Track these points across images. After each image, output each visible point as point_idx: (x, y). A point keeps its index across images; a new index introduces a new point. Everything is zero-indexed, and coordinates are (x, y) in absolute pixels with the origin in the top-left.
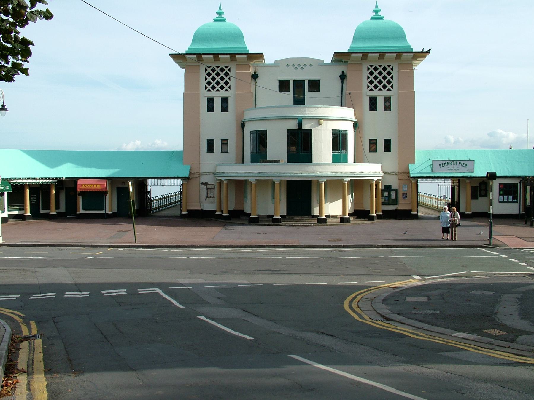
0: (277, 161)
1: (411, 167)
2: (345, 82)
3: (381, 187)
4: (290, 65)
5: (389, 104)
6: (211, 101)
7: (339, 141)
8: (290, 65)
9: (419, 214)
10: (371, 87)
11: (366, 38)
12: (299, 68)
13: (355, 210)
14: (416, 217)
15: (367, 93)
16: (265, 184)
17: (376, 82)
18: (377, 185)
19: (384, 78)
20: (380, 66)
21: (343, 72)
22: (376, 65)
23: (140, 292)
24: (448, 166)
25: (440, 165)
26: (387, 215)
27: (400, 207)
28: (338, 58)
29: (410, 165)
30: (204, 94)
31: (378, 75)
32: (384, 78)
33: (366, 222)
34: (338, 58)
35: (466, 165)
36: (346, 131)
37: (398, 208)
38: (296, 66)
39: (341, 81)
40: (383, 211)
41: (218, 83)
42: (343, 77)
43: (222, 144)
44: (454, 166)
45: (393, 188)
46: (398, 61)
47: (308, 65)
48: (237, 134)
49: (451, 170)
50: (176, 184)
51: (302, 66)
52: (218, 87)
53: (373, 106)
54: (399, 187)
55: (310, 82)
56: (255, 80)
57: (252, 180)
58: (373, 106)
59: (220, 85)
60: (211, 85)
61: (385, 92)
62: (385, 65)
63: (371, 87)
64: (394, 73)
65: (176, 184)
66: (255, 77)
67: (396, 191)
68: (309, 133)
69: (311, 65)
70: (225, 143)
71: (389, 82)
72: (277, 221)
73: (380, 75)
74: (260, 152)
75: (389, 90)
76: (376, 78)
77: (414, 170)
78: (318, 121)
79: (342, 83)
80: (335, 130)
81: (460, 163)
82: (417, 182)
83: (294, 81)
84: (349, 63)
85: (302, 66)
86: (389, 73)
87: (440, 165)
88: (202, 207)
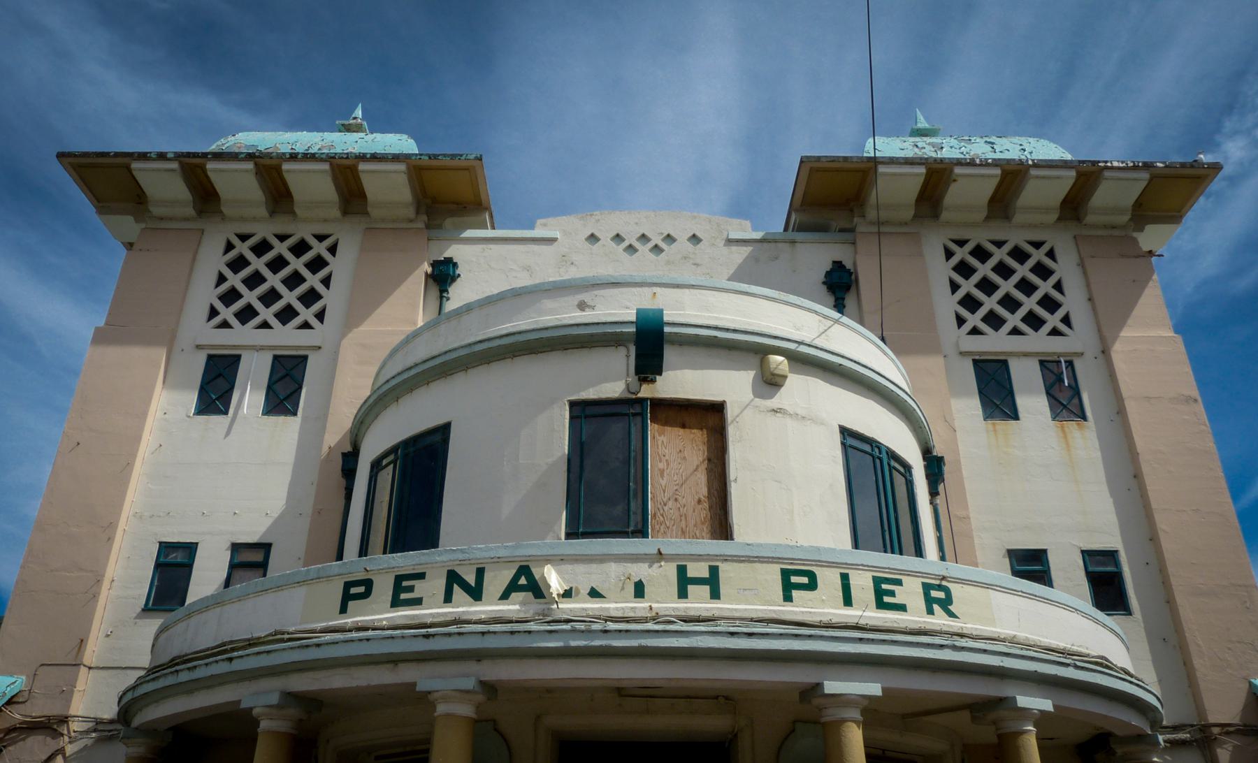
22: (980, 237)
47: (682, 237)
48: (318, 512)
61: (1039, 341)
62: (1017, 238)
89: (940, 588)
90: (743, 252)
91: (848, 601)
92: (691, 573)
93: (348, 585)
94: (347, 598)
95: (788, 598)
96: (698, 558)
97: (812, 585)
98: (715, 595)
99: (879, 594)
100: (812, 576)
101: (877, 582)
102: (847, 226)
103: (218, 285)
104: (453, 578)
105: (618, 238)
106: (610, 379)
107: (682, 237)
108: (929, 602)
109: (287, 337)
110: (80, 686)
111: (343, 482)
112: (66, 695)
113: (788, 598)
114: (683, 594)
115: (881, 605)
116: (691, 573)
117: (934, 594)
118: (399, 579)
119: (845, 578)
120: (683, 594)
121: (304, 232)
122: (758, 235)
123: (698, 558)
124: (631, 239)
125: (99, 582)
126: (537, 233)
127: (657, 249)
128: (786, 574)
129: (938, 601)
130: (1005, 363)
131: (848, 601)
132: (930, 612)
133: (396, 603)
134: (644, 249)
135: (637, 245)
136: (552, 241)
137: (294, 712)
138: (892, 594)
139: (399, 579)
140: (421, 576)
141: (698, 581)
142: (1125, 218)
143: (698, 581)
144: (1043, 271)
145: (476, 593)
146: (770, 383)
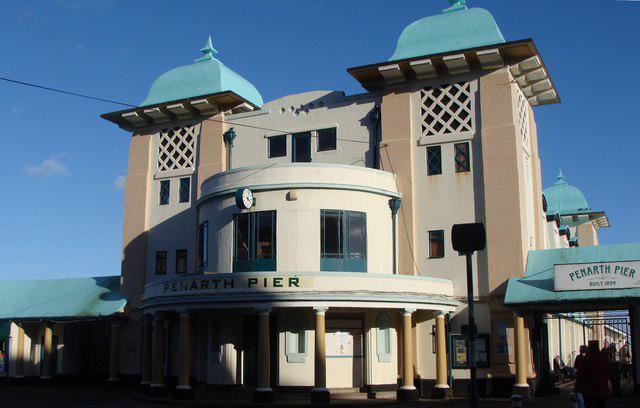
6: (165, 187)
7: (340, 237)
17: (438, 118)
19: (455, 107)
20: (469, 106)
23: (510, 332)
25: (571, 275)
35: (633, 272)
36: (365, 214)
41: (446, 117)
43: (178, 257)
44: (605, 275)
57: (322, 308)
66: (229, 137)
67: (486, 337)
68: (268, 220)
70: (181, 254)
76: (438, 110)
78: (290, 193)
80: (327, 212)
81: (617, 268)
83: (294, 135)
87: (571, 275)
98: (232, 287)
118: (275, 279)
139: (275, 279)
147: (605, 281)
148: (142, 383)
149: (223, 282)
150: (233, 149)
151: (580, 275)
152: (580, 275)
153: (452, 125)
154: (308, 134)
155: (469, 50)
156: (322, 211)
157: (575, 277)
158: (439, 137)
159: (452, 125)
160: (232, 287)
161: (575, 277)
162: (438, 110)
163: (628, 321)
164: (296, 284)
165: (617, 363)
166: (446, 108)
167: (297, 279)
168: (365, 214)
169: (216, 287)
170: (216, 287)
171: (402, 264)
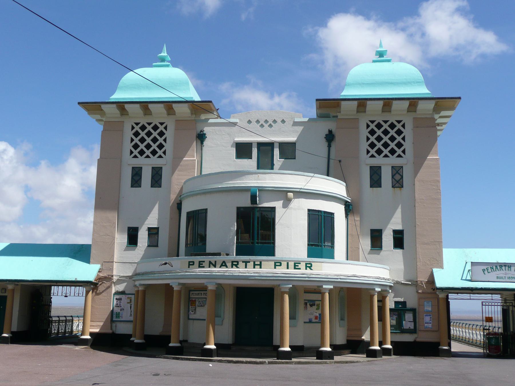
0: (243, 262)
1: (437, 272)
2: (333, 145)
3: (390, 304)
4: (254, 121)
5: (399, 177)
7: (320, 232)
8: (254, 121)
9: (452, 350)
10: (373, 152)
11: (363, 84)
12: (266, 125)
13: (348, 341)
14: (449, 354)
15: (366, 162)
16: (193, 294)
18: (382, 301)
20: (149, 124)
21: (330, 132)
22: (379, 119)
24: (498, 272)
25: (484, 270)
26: (401, 349)
27: (422, 337)
28: (324, 111)
29: (435, 270)
30: (129, 162)
31: (382, 136)
32: (155, 140)
33: (361, 358)
34: (324, 111)
36: (332, 214)
37: (418, 340)
38: (262, 122)
39: (326, 144)
40: (91, 334)
41: (386, 145)
42: (330, 137)
45: (409, 305)
46: (413, 115)
47: (279, 121)
48: (171, 219)
49: (501, 278)
50: (60, 294)
51: (270, 122)
52: (148, 152)
53: (376, 181)
54: (419, 305)
55: (260, 145)
56: (202, 143)
58: (376, 181)
59: (389, 148)
60: (396, 148)
61: (393, 160)
62: (392, 120)
63: (373, 152)
64: (169, 134)
65: (60, 294)
69: (283, 121)
71: (161, 146)
72: (209, 353)
73: (386, 136)
74: (198, 245)
75: (399, 156)
77: (443, 279)
78: (284, 195)
79: (329, 146)
82: (447, 297)
84: (339, 117)
85: (270, 122)
86: (399, 132)
88: (114, 329)
89: (309, 264)
90: (300, 129)
91: (288, 268)
92: (256, 263)
93: (189, 262)
94: (189, 265)
95: (275, 268)
96: (257, 261)
97: (280, 265)
98: (261, 268)
99: (295, 266)
100: (281, 263)
101: (295, 264)
102: (335, 115)
103: (131, 142)
104: (210, 263)
105: (258, 121)
106: (246, 202)
107: (279, 121)
108: (306, 267)
109: (155, 161)
110: (114, 267)
111: (177, 211)
112: (112, 270)
113: (275, 268)
114: (254, 267)
115: (295, 268)
116: (256, 263)
117: (308, 265)
118: (200, 262)
119: (288, 263)
120: (254, 267)
121: (156, 122)
122: (306, 120)
123: (257, 261)
124: (262, 122)
125: (114, 239)
126: (232, 120)
127: (270, 126)
128: (275, 263)
129: (308, 267)
130: (380, 167)
131: (288, 268)
132: (306, 269)
133: (199, 267)
134: (266, 125)
135: (264, 124)
136: (235, 124)
137: (180, 286)
138: (298, 266)
139: (200, 262)
140: (204, 262)
141: (257, 265)
142: (431, 112)
143: (257, 265)
144: (399, 132)
145: (215, 266)
146: (287, 202)
147: (508, 276)
148: (171, 345)
149: (252, 263)
150: (204, 148)
151: (490, 271)
152: (490, 271)
153: (139, 153)
154: (271, 145)
155: (413, 99)
156: (238, 209)
157: (486, 272)
158: (378, 161)
159: (139, 153)
160: (261, 268)
161: (486, 272)
162: (155, 140)
163: (514, 304)
164: (310, 268)
165: (363, 341)
166: (149, 140)
167: (311, 265)
168: (332, 214)
169: (246, 267)
170: (246, 267)
171: (351, 255)
